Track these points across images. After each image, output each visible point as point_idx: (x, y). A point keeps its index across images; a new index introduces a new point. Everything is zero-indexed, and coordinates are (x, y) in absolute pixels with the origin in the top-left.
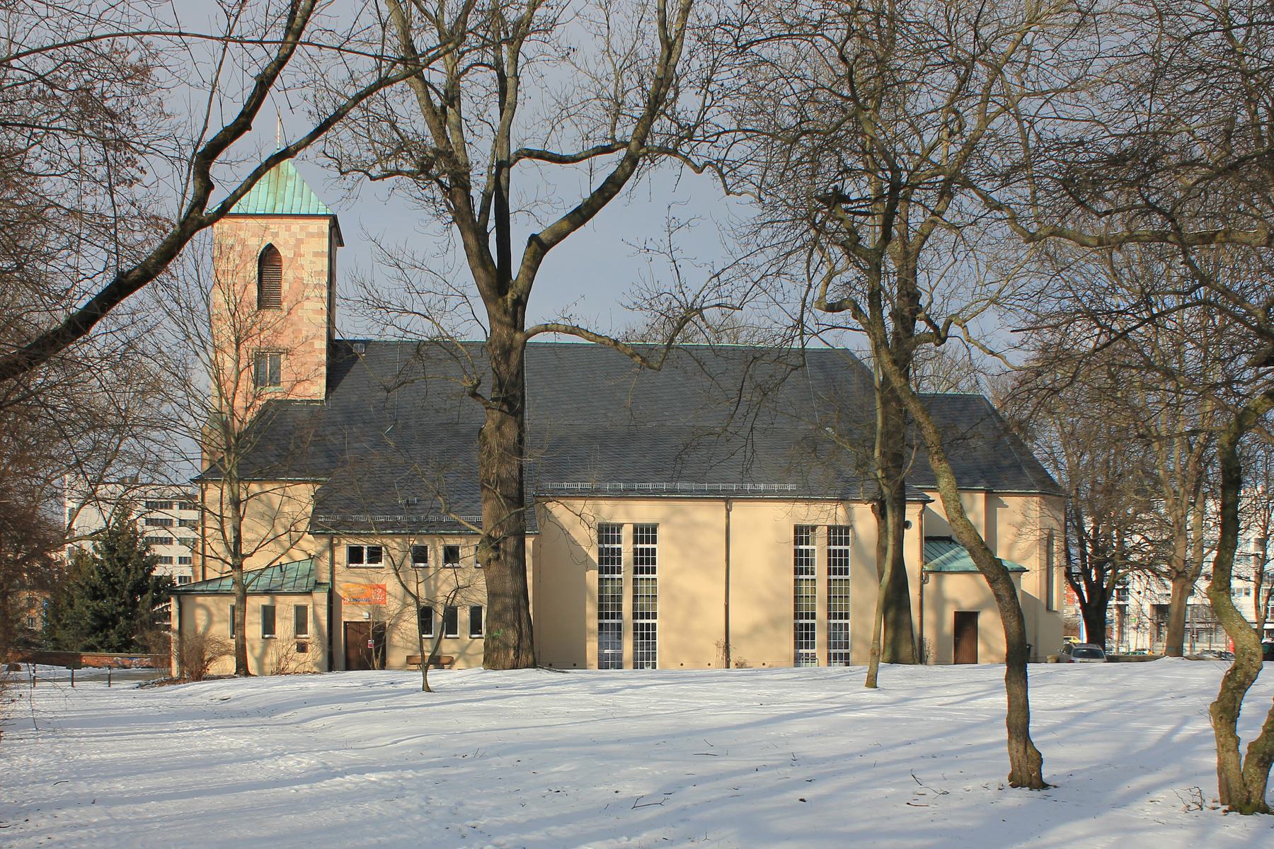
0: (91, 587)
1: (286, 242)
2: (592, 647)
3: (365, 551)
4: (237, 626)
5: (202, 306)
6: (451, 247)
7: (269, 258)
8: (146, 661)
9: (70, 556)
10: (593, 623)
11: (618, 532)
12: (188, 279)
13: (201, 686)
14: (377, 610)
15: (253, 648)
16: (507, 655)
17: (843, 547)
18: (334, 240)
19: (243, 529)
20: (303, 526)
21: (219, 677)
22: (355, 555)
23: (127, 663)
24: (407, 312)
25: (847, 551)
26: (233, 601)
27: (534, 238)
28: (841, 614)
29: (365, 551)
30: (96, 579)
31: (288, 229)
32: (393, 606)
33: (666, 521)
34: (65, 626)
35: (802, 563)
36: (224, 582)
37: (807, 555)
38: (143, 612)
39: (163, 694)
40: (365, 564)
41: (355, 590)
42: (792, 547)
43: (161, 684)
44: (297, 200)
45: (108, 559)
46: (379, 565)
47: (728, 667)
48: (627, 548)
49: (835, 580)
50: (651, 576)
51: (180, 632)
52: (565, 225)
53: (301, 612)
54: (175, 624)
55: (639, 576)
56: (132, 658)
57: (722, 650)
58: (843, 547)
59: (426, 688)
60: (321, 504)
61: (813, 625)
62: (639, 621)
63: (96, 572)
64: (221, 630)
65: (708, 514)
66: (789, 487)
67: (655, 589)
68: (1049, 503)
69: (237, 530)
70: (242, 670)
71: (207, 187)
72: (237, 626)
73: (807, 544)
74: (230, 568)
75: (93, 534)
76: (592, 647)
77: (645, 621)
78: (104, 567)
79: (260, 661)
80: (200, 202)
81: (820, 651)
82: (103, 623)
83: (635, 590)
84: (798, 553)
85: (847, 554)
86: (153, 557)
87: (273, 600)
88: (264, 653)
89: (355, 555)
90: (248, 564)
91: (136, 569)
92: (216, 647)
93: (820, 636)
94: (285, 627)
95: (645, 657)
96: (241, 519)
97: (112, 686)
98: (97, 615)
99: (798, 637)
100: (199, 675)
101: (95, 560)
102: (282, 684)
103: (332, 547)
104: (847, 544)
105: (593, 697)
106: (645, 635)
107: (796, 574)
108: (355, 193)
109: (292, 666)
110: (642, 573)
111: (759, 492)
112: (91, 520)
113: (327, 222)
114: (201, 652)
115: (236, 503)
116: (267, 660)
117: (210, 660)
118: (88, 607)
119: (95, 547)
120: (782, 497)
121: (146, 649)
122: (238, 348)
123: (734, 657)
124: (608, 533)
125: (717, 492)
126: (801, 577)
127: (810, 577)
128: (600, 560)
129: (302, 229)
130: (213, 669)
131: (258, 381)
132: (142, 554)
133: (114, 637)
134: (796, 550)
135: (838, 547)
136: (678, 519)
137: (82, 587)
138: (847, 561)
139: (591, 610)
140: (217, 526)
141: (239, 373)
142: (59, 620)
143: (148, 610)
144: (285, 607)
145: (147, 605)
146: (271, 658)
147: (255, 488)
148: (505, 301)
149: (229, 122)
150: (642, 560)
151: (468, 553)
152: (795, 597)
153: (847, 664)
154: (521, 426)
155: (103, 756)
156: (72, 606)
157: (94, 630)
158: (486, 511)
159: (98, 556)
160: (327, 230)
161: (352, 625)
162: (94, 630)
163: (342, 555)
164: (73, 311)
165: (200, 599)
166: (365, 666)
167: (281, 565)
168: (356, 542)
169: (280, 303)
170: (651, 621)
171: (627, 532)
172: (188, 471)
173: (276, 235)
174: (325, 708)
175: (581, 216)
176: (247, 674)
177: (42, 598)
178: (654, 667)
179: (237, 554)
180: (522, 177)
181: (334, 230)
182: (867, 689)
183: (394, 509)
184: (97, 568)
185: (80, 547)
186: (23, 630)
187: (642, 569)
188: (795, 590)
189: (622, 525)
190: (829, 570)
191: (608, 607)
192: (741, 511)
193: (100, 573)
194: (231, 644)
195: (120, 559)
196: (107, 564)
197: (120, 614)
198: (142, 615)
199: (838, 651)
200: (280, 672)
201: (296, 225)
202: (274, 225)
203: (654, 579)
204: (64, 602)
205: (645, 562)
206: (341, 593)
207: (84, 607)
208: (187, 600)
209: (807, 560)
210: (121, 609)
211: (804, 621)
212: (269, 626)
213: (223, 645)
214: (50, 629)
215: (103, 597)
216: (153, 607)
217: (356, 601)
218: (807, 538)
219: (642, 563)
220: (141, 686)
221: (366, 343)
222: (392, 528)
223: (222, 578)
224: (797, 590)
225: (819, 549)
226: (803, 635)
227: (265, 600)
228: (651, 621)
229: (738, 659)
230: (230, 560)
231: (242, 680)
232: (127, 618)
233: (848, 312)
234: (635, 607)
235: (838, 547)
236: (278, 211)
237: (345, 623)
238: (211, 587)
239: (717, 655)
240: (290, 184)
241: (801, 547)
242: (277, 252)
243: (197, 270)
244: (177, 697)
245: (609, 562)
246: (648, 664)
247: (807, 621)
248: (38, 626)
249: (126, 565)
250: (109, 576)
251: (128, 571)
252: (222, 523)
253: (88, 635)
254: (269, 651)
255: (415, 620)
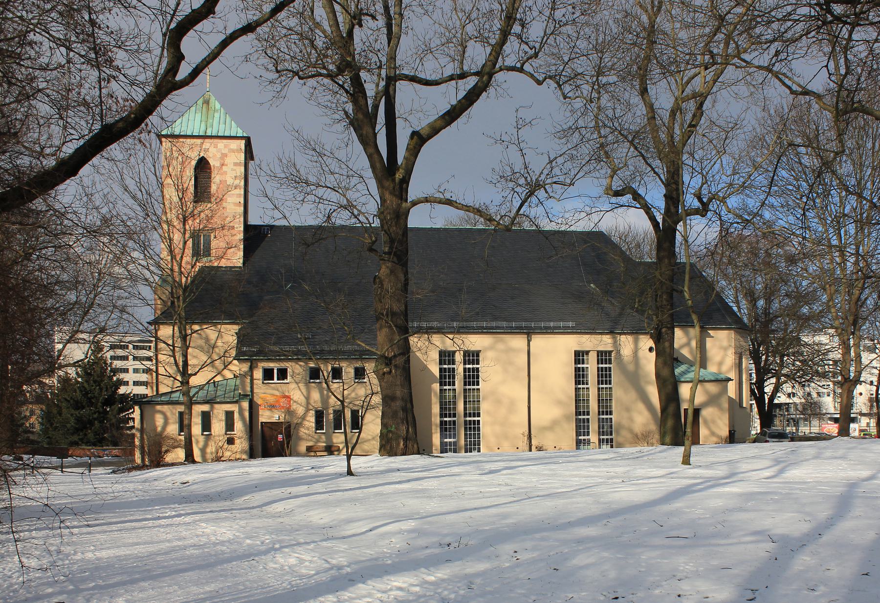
0: (74, 400)
1: (214, 156)
2: (436, 439)
3: (275, 371)
4: (184, 426)
5: (158, 193)
6: (350, 142)
7: (202, 166)
8: (115, 452)
9: (59, 382)
10: (436, 420)
11: (453, 357)
12: (148, 172)
13: (162, 472)
14: (289, 412)
15: (197, 442)
16: (399, 444)
17: (607, 366)
18: (248, 156)
19: (189, 357)
20: (233, 353)
21: (173, 465)
22: (268, 374)
23: (101, 454)
24: (321, 186)
25: (610, 368)
26: (182, 408)
27: (414, 134)
28: (474, 414)
29: (275, 371)
30: (78, 395)
31: (216, 147)
32: (301, 411)
33: (491, 348)
34: (56, 428)
35: (580, 376)
36: (173, 395)
37: (583, 371)
38: (112, 417)
39: (133, 479)
40: (275, 380)
41: (271, 400)
42: (574, 366)
43: (130, 470)
44: (222, 126)
45: (87, 381)
46: (285, 381)
47: (530, 450)
48: (460, 369)
49: (603, 388)
50: (476, 387)
51: (142, 430)
52: (439, 124)
53: (229, 415)
54: (137, 424)
55: (468, 387)
56: (105, 450)
57: (526, 438)
58: (607, 366)
59: (350, 473)
60: (241, 337)
61: (588, 420)
62: (468, 419)
63: (78, 391)
64: (173, 429)
65: (518, 342)
66: (570, 324)
67: (478, 396)
68: (739, 333)
69: (185, 356)
70: (190, 458)
71: (178, 58)
72: (184, 426)
73: (583, 363)
74: (179, 384)
75: (76, 363)
76: (436, 439)
77: (472, 419)
78: (83, 387)
79: (203, 451)
80: (173, 68)
81: (593, 437)
82: (83, 425)
83: (465, 397)
84: (577, 370)
85: (610, 370)
86: (118, 380)
87: (212, 408)
88: (206, 445)
89: (268, 374)
90: (194, 381)
91: (107, 388)
92: (171, 442)
93: (594, 426)
94: (218, 427)
95: (473, 445)
96: (188, 348)
97: (92, 472)
98: (79, 420)
99: (578, 427)
100: (157, 461)
101: (78, 382)
102: (225, 469)
103: (251, 369)
104: (610, 363)
105: (484, 477)
106: (473, 428)
107: (576, 384)
108: (283, 93)
109: (227, 454)
110: (469, 385)
111: (549, 328)
112: (77, 352)
113: (244, 142)
114: (160, 445)
115: (184, 338)
116: (209, 450)
117: (167, 451)
118: (72, 415)
119: (77, 373)
120: (566, 331)
121: (115, 444)
122: (184, 225)
123: (534, 442)
124: (446, 357)
125: (521, 328)
126: (579, 386)
127: (585, 386)
128: (440, 376)
129: (226, 146)
130: (169, 458)
131: (196, 253)
132: (111, 378)
133: (91, 435)
134: (575, 368)
135: (604, 366)
136: (500, 346)
137: (69, 401)
138: (610, 375)
139: (436, 409)
140: (171, 353)
141: (185, 243)
142: (52, 424)
143: (115, 416)
144: (219, 411)
145: (115, 412)
146: (211, 449)
147: (196, 327)
148: (394, 180)
149: (196, 6)
150: (469, 376)
151: (369, 367)
152: (576, 400)
153: (612, 447)
154: (406, 273)
155: (98, 554)
156: (60, 414)
157: (77, 431)
158: (382, 336)
159: (80, 380)
160: (243, 147)
161: (268, 425)
162: (77, 431)
163: (258, 374)
164: (62, 155)
165: (159, 407)
166: (280, 453)
167: (214, 382)
168: (271, 365)
169: (210, 198)
170: (476, 419)
171: (459, 357)
172: (147, 314)
173: (207, 150)
174: (276, 492)
175: (452, 116)
176: (194, 462)
177: (37, 409)
178: (479, 451)
179: (185, 373)
180: (404, 91)
181: (248, 148)
182: (683, 466)
183: (299, 342)
184: (78, 387)
185: (67, 373)
186: (27, 431)
187: (469, 382)
188: (576, 395)
189: (454, 352)
190: (598, 381)
191: (447, 408)
192: (538, 341)
193: (81, 391)
194: (181, 440)
195: (95, 382)
196: (86, 385)
197: (95, 419)
198: (111, 419)
199: (605, 437)
200: (218, 459)
201: (221, 143)
202: (207, 143)
203: (478, 389)
204: (55, 411)
205: (472, 377)
206: (259, 402)
207: (69, 416)
208: (147, 408)
209: (583, 375)
210: (95, 416)
211: (581, 417)
212: (206, 425)
213: (175, 440)
214: (45, 431)
215: (83, 408)
216: (119, 414)
217: (272, 407)
218: (583, 360)
219: (473, 376)
220: (114, 472)
221: (272, 227)
222: (296, 355)
223: (172, 392)
224: (577, 396)
225: (591, 366)
226: (581, 428)
227: (206, 408)
228: (476, 419)
229: (537, 444)
230: (179, 378)
231: (191, 467)
232: (100, 422)
233: (629, 196)
234: (465, 409)
235: (604, 366)
236: (209, 133)
237: (262, 423)
238: (163, 398)
239: (523, 443)
240: (217, 115)
241: (579, 366)
242: (208, 163)
243: (154, 166)
244: (145, 481)
245: (447, 377)
246: (475, 449)
247: (584, 417)
248: (38, 428)
249: (99, 385)
250: (87, 393)
251: (101, 389)
252: (173, 351)
253: (73, 434)
254: (210, 443)
255: (313, 419)
